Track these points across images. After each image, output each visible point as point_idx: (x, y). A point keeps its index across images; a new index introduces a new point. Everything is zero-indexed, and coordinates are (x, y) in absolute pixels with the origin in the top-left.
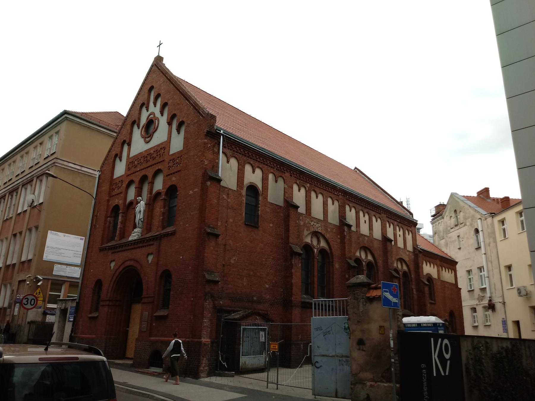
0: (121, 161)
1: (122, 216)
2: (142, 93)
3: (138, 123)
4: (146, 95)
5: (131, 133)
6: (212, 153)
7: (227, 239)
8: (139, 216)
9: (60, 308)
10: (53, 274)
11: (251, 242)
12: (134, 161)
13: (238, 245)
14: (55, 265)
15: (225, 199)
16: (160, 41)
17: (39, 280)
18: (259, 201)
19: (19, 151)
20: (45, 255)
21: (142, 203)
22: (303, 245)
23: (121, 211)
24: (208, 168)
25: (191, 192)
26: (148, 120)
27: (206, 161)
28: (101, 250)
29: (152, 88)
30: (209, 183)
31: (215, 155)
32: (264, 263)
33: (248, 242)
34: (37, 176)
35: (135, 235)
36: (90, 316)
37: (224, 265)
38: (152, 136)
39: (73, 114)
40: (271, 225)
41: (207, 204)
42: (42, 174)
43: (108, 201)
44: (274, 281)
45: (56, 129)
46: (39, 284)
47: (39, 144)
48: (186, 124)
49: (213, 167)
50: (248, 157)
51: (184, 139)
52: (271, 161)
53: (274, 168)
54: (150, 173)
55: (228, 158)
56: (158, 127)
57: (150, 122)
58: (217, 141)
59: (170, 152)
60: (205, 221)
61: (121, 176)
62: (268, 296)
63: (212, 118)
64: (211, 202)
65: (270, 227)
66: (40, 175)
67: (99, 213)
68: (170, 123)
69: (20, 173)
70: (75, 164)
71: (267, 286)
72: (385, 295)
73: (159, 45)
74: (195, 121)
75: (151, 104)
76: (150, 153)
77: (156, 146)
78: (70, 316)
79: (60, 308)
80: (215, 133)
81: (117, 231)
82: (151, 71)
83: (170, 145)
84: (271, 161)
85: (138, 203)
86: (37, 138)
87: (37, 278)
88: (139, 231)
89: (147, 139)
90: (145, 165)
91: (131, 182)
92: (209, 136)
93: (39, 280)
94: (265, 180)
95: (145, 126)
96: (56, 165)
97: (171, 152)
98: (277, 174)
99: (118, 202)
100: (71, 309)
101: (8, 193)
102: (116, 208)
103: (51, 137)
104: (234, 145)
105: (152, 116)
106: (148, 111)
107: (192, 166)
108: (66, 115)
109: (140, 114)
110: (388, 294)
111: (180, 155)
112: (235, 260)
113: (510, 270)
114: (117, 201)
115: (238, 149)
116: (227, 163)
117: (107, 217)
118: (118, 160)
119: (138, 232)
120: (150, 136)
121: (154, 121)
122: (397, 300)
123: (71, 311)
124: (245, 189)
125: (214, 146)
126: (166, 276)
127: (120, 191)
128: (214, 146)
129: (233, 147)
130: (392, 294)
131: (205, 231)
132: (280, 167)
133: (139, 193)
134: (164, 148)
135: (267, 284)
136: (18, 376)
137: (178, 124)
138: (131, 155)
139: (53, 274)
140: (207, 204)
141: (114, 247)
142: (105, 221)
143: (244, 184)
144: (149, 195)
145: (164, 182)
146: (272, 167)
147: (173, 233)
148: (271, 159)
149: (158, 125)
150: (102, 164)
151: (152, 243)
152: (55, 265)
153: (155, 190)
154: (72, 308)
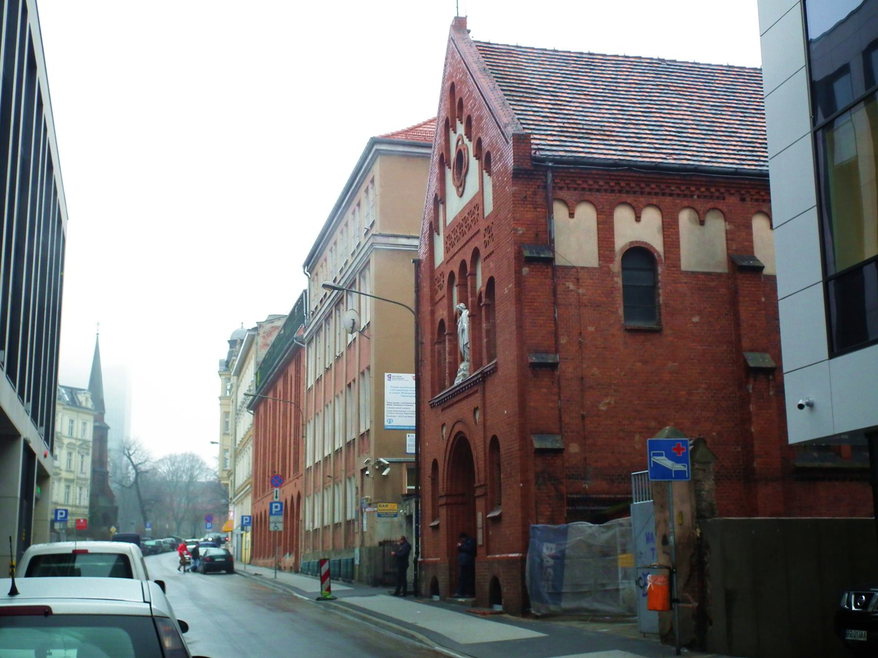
0: (438, 234)
1: (449, 340)
6: (533, 210)
7: (584, 366)
8: (464, 339)
9: (405, 514)
10: (407, 452)
14: (408, 434)
15: (571, 291)
17: (383, 467)
18: (659, 274)
19: (336, 222)
20: (386, 418)
27: (519, 228)
30: (525, 270)
31: (538, 210)
33: (639, 364)
34: (359, 271)
37: (583, 417)
39: (388, 139)
40: (696, 319)
42: (364, 265)
44: (714, 434)
46: (385, 473)
49: (537, 235)
50: (620, 192)
52: (681, 184)
53: (692, 196)
55: (571, 208)
57: (460, 155)
58: (540, 181)
64: (535, 304)
65: (693, 323)
66: (362, 268)
69: (344, 266)
70: (408, 237)
72: (657, 461)
79: (405, 514)
83: (483, 200)
84: (681, 184)
86: (351, 194)
87: (380, 462)
88: (465, 366)
93: (383, 467)
94: (670, 229)
96: (376, 248)
98: (701, 205)
101: (334, 307)
104: (579, 177)
106: (455, 132)
108: (376, 147)
110: (664, 458)
112: (609, 403)
113: (68, 489)
115: (591, 182)
116: (570, 217)
119: (464, 370)
122: (685, 466)
124: (618, 258)
126: (494, 443)
129: (578, 182)
130: (671, 457)
132: (708, 189)
134: (477, 207)
139: (407, 452)
143: (614, 251)
146: (685, 196)
147: (495, 370)
148: (676, 179)
152: (408, 434)
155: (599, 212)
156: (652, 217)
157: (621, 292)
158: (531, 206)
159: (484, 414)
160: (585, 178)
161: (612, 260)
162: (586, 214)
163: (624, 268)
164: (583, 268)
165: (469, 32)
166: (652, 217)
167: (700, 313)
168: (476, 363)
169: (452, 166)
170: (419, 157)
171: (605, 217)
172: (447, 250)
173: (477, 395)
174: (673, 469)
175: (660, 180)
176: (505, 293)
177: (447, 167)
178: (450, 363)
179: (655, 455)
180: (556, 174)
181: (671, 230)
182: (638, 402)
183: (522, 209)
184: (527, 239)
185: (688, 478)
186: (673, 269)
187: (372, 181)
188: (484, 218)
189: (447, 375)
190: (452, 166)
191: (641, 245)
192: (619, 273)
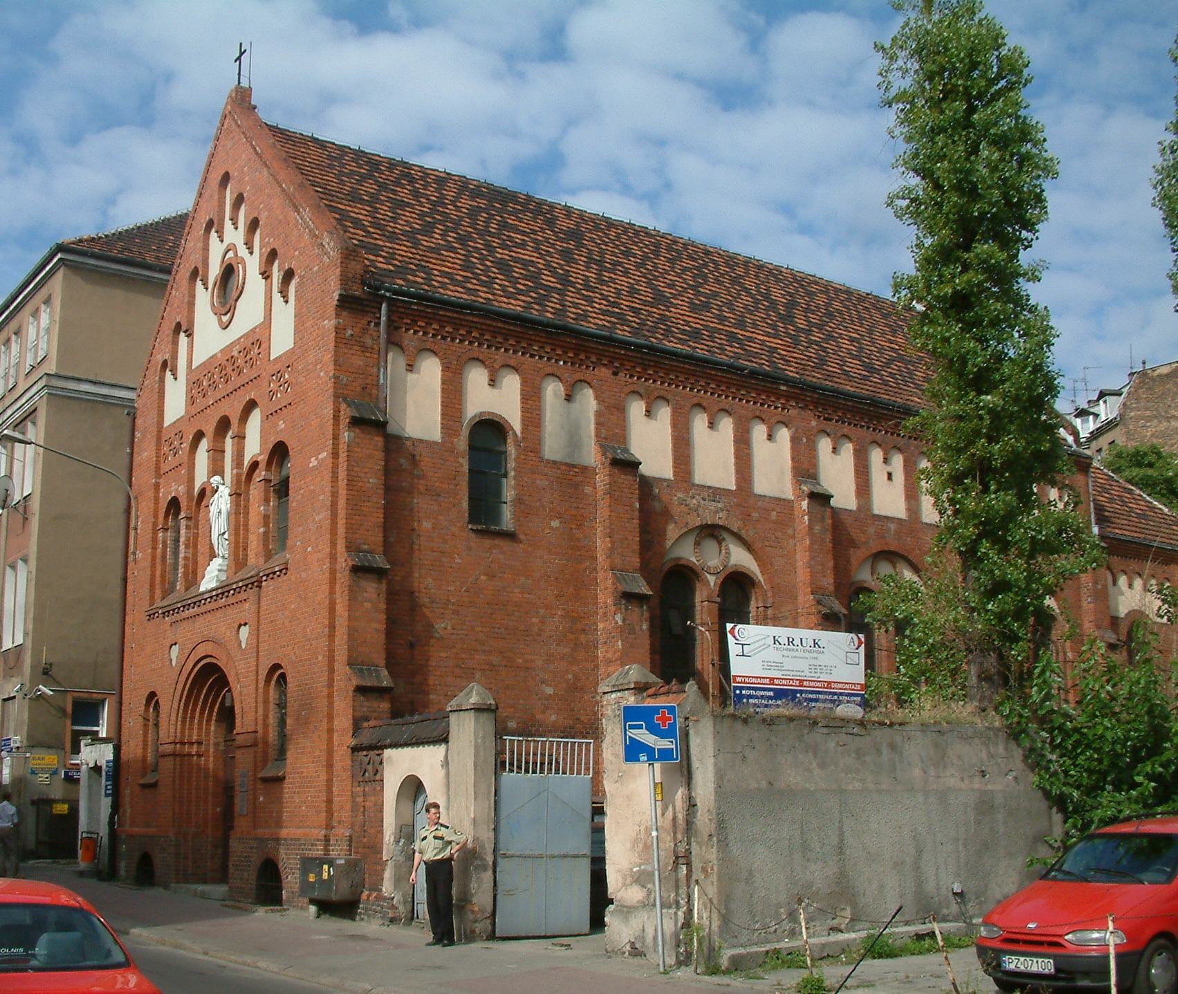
2: (206, 194)
3: (202, 276)
5: (191, 304)
11: (491, 577)
13: (452, 588)
16: (241, 44)
21: (224, 491)
22: (666, 568)
23: (182, 515)
24: (350, 392)
26: (224, 266)
29: (226, 178)
32: (536, 629)
33: (483, 578)
35: (212, 576)
36: (143, 781)
40: (555, 524)
42: (22, 418)
43: (157, 487)
45: (43, 294)
47: (13, 336)
48: (297, 277)
51: (295, 317)
54: (233, 409)
56: (244, 283)
57: (228, 272)
58: (372, 315)
59: (271, 354)
61: (178, 420)
62: (553, 717)
63: (352, 257)
64: (360, 484)
65: (552, 528)
68: (266, 275)
70: (95, 383)
71: (549, 690)
72: (633, 736)
73: (238, 55)
75: (228, 224)
76: (232, 357)
77: (241, 337)
80: (362, 297)
81: (180, 567)
89: (225, 319)
90: (223, 389)
91: (199, 435)
92: (347, 308)
94: (531, 399)
95: (218, 283)
99: (177, 490)
103: (36, 313)
105: (230, 254)
109: (206, 249)
110: (644, 731)
111: (289, 361)
120: (230, 309)
121: (235, 268)
122: (672, 742)
124: (465, 432)
125: (365, 330)
126: (277, 675)
128: (365, 330)
133: (216, 468)
134: (259, 343)
135: (550, 686)
136: (1118, 942)
137: (281, 277)
144: (235, 471)
155: (446, 368)
156: (512, 383)
157: (466, 478)
158: (358, 348)
159: (257, 633)
160: (430, 318)
161: (456, 434)
162: (431, 370)
163: (472, 448)
164: (421, 441)
165: (255, 108)
166: (512, 383)
167: (559, 516)
168: (238, 559)
169: (210, 286)
170: (115, 275)
171: (451, 375)
172: (191, 400)
173: (247, 605)
174: (657, 747)
175: (520, 335)
176: (311, 465)
177: (199, 283)
178: (186, 558)
179: (631, 727)
180: (394, 309)
181: (530, 402)
182: (480, 629)
183: (346, 351)
184: (350, 392)
185: (677, 759)
186: (530, 454)
187: (47, 301)
188: (269, 360)
189: (180, 575)
190: (210, 286)
191: (495, 419)
192: (465, 451)
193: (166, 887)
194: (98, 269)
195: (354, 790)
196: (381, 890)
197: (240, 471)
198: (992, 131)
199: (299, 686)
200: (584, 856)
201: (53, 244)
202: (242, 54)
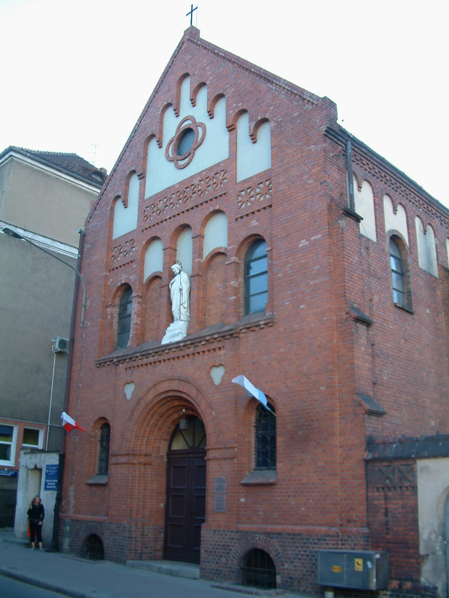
2: (165, 88)
4: (174, 90)
6: (337, 170)
12: (156, 202)
16: (192, 5)
23: (134, 294)
25: (303, 243)
28: (101, 364)
33: (402, 341)
38: (191, 155)
41: (345, 263)
60: (345, 296)
64: (351, 259)
67: (89, 300)
68: (231, 128)
73: (193, 12)
74: (295, 115)
77: (203, 171)
78: (47, 481)
82: (180, 52)
85: (172, 275)
89: (181, 163)
90: (180, 207)
95: (174, 142)
97: (240, 179)
100: (47, 469)
102: (127, 288)
105: (188, 122)
107: (300, 194)
114: (124, 277)
117: (106, 306)
118: (119, 204)
123: (49, 472)
127: (128, 259)
131: (348, 316)
138: (149, 194)
140: (345, 263)
141: (131, 359)
142: (104, 315)
145: (231, 232)
149: (204, 138)
150: (88, 217)
151: (216, 345)
153: (208, 249)
154: (51, 468)
158: (336, 167)
169: (165, 144)
193: (121, 561)
194: (45, 162)
195: (370, 494)
196: (418, 581)
197: (200, 260)
198: (126, 350)
199: (294, 411)
200: (113, 456)
201: (7, 147)
202: (192, 11)
